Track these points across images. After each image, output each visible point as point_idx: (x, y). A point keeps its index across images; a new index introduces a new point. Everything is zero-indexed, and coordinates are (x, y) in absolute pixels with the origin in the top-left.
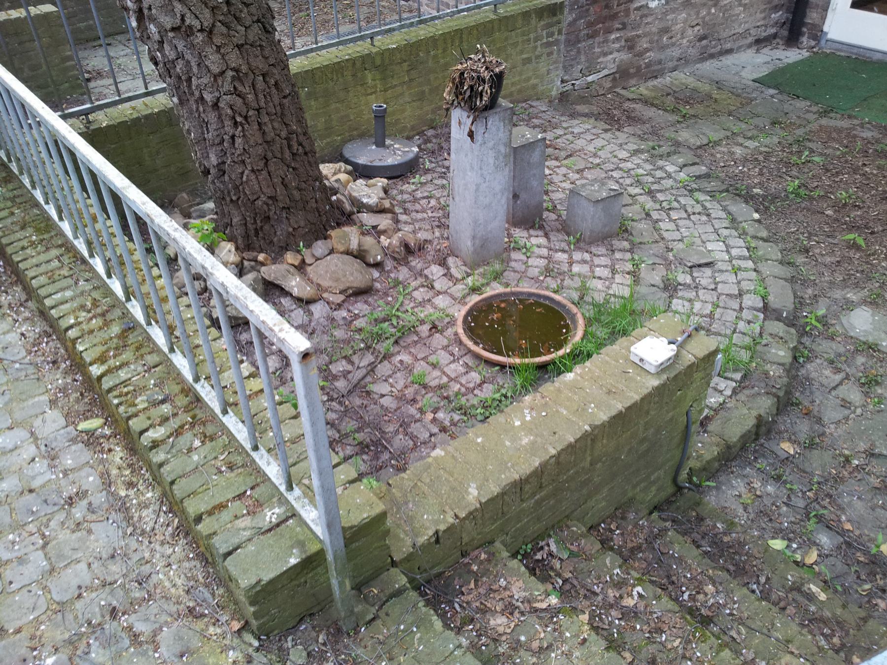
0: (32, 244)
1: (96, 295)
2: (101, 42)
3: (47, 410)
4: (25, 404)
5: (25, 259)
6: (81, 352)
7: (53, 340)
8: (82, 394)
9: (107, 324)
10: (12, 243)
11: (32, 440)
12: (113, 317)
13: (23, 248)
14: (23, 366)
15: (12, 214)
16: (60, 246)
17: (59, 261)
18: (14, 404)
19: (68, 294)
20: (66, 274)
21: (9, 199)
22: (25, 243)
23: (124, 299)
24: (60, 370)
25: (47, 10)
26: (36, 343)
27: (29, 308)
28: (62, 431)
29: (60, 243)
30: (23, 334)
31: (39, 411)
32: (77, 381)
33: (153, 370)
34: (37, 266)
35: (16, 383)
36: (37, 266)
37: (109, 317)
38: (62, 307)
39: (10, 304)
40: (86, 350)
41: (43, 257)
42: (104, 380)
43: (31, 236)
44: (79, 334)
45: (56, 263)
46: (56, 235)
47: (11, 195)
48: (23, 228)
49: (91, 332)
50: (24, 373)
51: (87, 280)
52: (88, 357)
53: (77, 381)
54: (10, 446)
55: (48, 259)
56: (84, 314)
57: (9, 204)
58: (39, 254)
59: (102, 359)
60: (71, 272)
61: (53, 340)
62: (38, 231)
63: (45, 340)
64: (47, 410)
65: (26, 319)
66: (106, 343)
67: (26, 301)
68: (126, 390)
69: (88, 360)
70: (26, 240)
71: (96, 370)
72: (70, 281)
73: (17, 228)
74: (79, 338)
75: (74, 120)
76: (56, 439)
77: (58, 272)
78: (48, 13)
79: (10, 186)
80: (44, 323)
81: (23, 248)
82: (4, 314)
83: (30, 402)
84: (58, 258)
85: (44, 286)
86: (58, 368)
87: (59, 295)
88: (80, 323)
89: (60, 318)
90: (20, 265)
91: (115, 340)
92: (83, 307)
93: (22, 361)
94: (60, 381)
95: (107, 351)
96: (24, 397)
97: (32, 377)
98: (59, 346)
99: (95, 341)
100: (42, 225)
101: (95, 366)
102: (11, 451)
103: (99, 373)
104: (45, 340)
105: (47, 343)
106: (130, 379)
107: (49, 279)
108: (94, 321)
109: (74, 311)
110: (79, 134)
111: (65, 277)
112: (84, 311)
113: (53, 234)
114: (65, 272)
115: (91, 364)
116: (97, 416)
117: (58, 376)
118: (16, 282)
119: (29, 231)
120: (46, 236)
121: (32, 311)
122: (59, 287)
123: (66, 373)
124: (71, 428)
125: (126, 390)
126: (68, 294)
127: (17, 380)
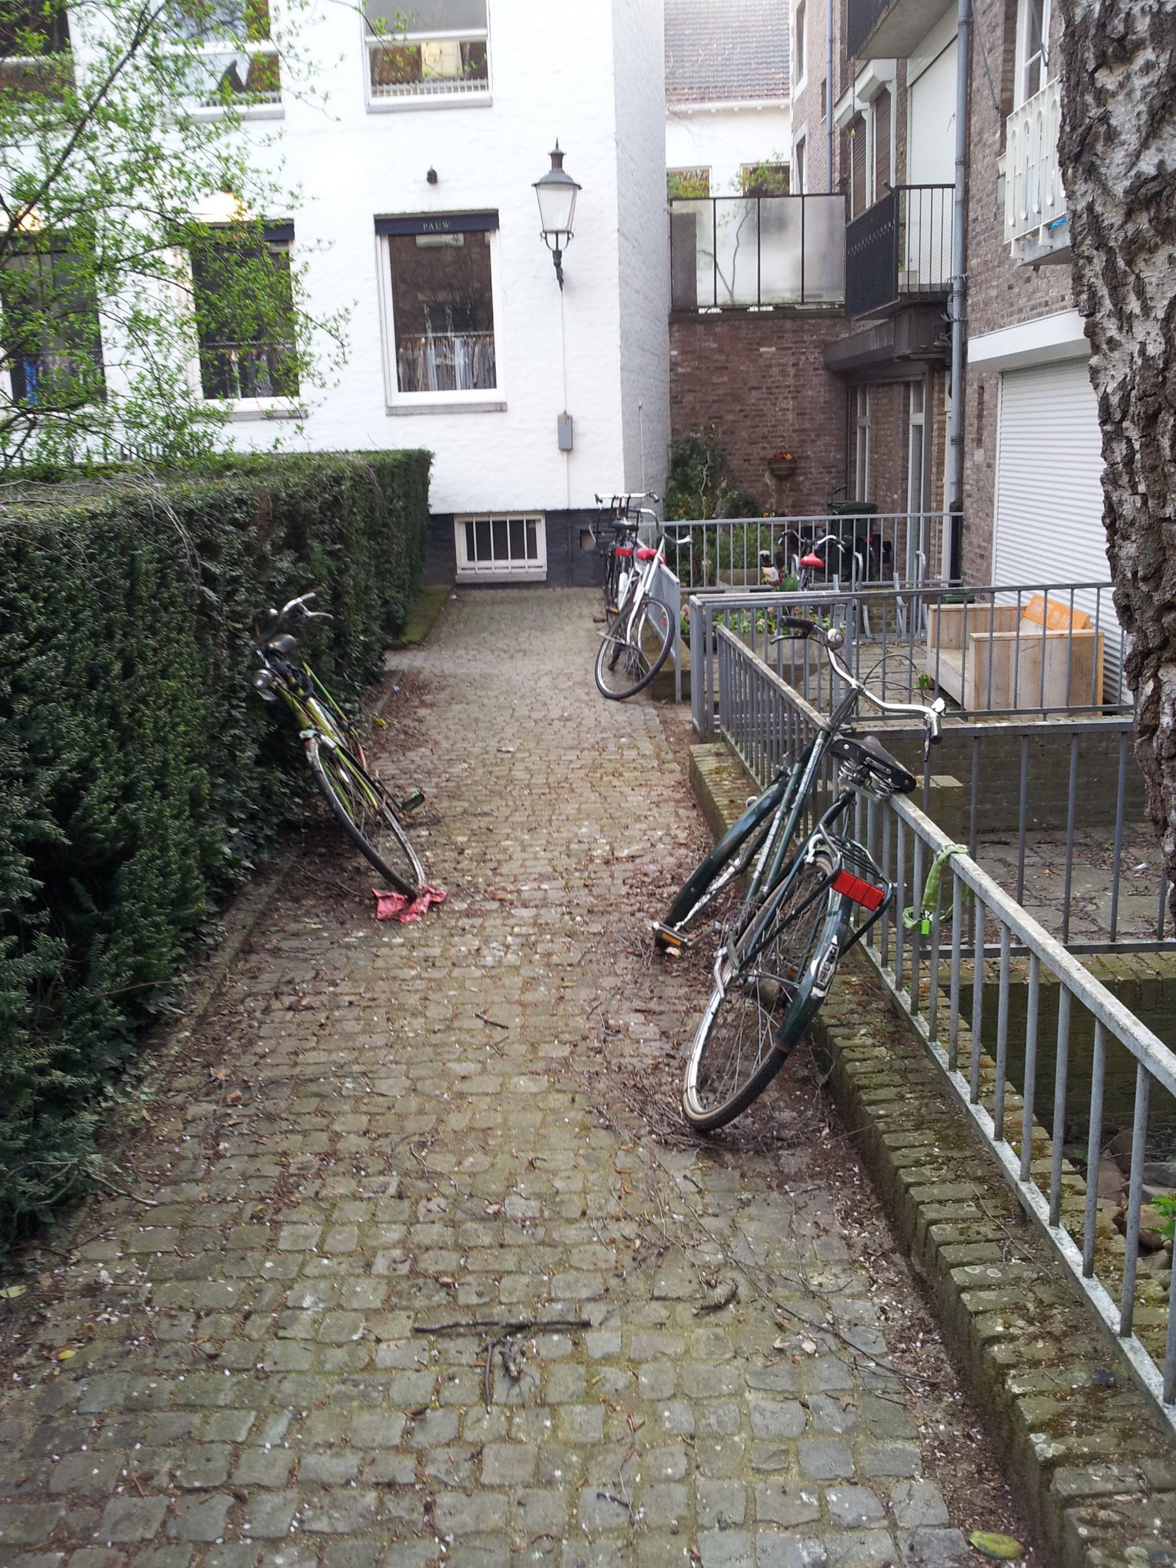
0: (933, 1159)
1: (1044, 1292)
2: (1066, 836)
3: (917, 1474)
4: (880, 1445)
5: (919, 1184)
6: (1016, 1396)
7: (934, 1341)
8: (980, 1472)
9: (1063, 1359)
10: (899, 1148)
11: (885, 1523)
12: (1075, 1350)
13: (918, 1163)
14: (880, 1370)
15: (902, 1098)
16: (980, 1180)
17: (978, 1206)
18: (861, 1438)
19: (993, 1273)
20: (990, 1236)
21: (898, 1071)
22: (920, 1154)
23: (1117, 1328)
24: (943, 1405)
25: (946, 784)
26: (905, 1336)
27: (895, 1265)
28: (942, 1532)
29: (979, 1173)
30: (883, 1311)
31: (903, 1471)
32: (972, 1440)
33: (1156, 1496)
34: (940, 1202)
35: (866, 1399)
36: (940, 1202)
37: (1069, 1346)
38: (984, 1295)
39: (866, 1246)
40: (1024, 1395)
41: (949, 1191)
42: (1060, 1472)
43: (931, 1145)
44: (1013, 1360)
45: (970, 1209)
46: (973, 1158)
47: (898, 1064)
48: (918, 1127)
49: (1035, 1363)
50: (881, 1385)
51: (1024, 1259)
52: (1030, 1411)
53: (972, 1440)
54: (849, 1518)
55: (959, 1196)
56: (1021, 1323)
57: (897, 1079)
58: (943, 1182)
59: (1054, 1427)
60: (998, 1235)
61: (934, 1341)
62: (943, 1139)
63: (921, 1335)
64: (917, 1474)
65: (890, 1284)
66: (1063, 1399)
67: (893, 1251)
68: (1102, 1514)
69: (1029, 1418)
70: (924, 1150)
71: (1044, 1446)
72: (991, 1250)
73: (909, 1125)
74: (1013, 1366)
75: (1086, 957)
76: (929, 1543)
77: (975, 1227)
78: (946, 788)
79: (901, 1050)
80: (921, 1304)
81: (918, 1163)
82: (855, 1261)
83: (890, 1446)
84: (976, 1199)
85: (949, 1243)
86: (939, 1399)
87: (976, 1270)
88: (1013, 1339)
89: (977, 1313)
90: (912, 1191)
91: (1081, 1400)
92: (1019, 1309)
93: (881, 1361)
94: (942, 1427)
95: (1067, 1413)
96: (879, 1431)
97: (895, 1398)
98: (943, 1356)
99: (1045, 1385)
100: (950, 1132)
101: (1042, 1436)
102: (851, 1528)
103: (1050, 1453)
104: (921, 1335)
105: (923, 1342)
106: (1110, 1494)
107: (961, 1234)
108: (1040, 1344)
109: (1003, 1310)
110: (1102, 982)
111: (988, 1241)
112: (1022, 1317)
113: (968, 1154)
114: (987, 1230)
115: (1033, 1428)
116: (1006, 1532)
117: (939, 1416)
118: (879, 1210)
119: (928, 1136)
120: (955, 1154)
121: (900, 1272)
122: (977, 1254)
123: (953, 1415)
124: (956, 1532)
125: (1102, 1514)
126: (993, 1273)
127: (869, 1392)
